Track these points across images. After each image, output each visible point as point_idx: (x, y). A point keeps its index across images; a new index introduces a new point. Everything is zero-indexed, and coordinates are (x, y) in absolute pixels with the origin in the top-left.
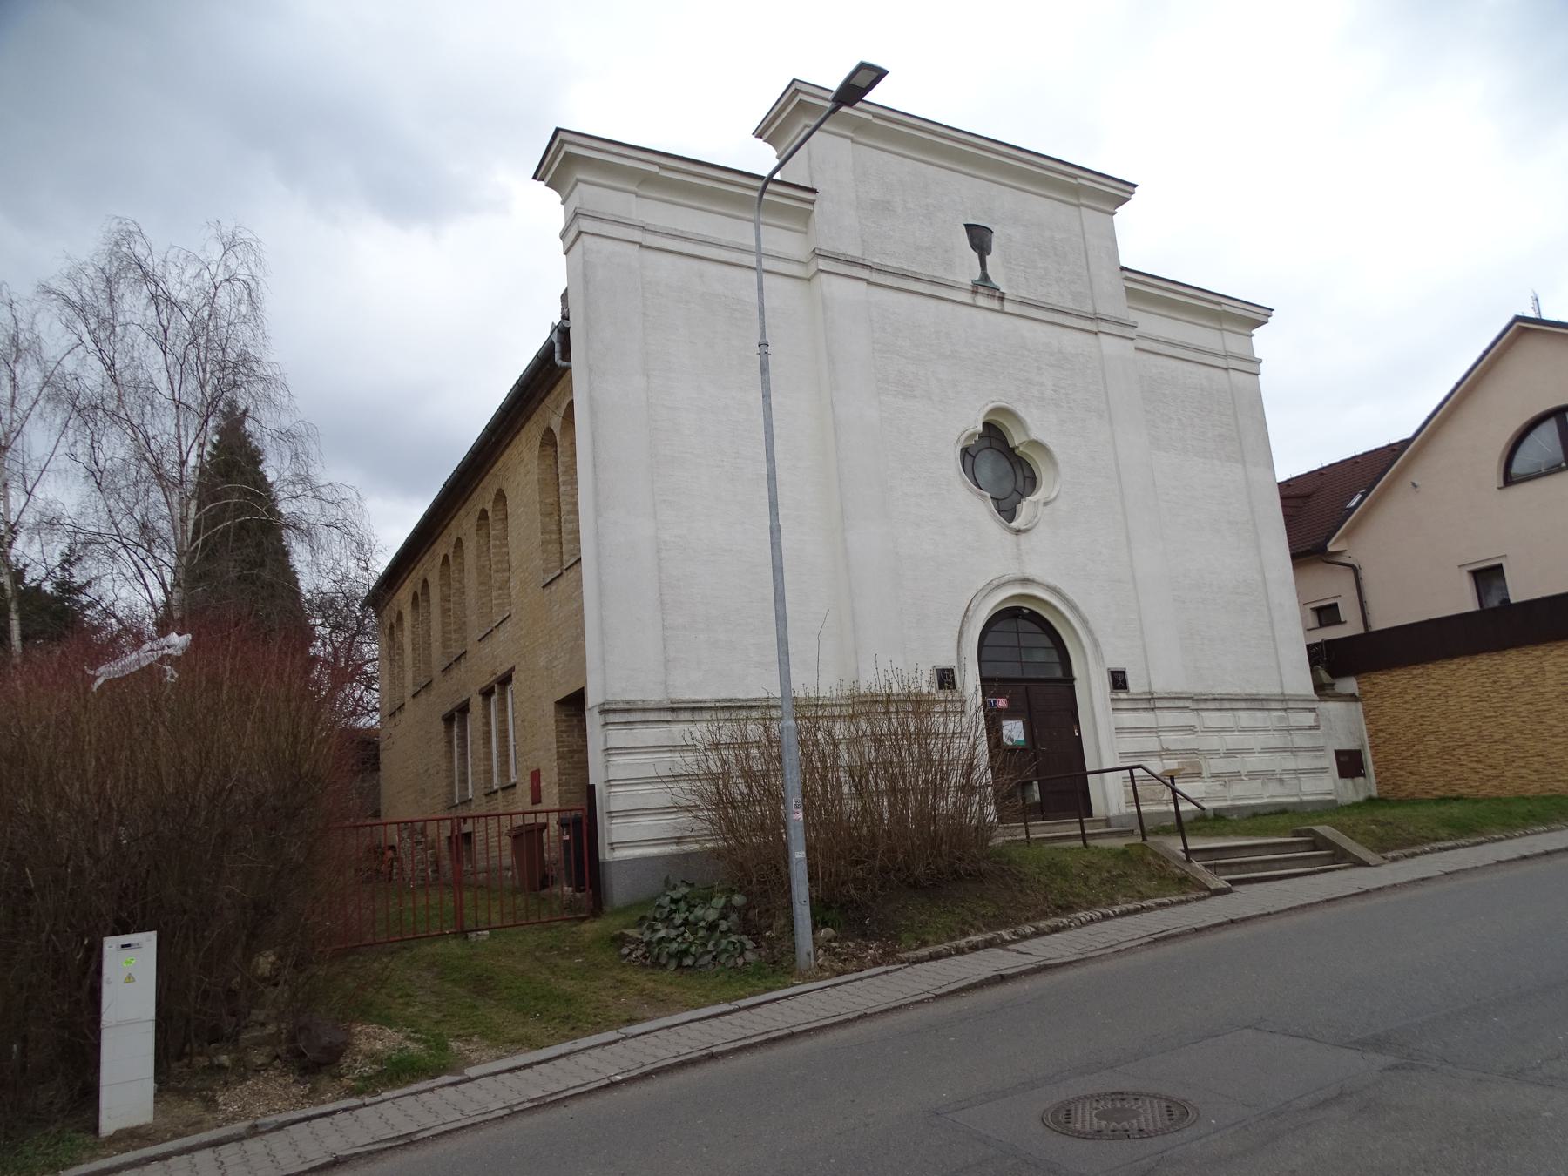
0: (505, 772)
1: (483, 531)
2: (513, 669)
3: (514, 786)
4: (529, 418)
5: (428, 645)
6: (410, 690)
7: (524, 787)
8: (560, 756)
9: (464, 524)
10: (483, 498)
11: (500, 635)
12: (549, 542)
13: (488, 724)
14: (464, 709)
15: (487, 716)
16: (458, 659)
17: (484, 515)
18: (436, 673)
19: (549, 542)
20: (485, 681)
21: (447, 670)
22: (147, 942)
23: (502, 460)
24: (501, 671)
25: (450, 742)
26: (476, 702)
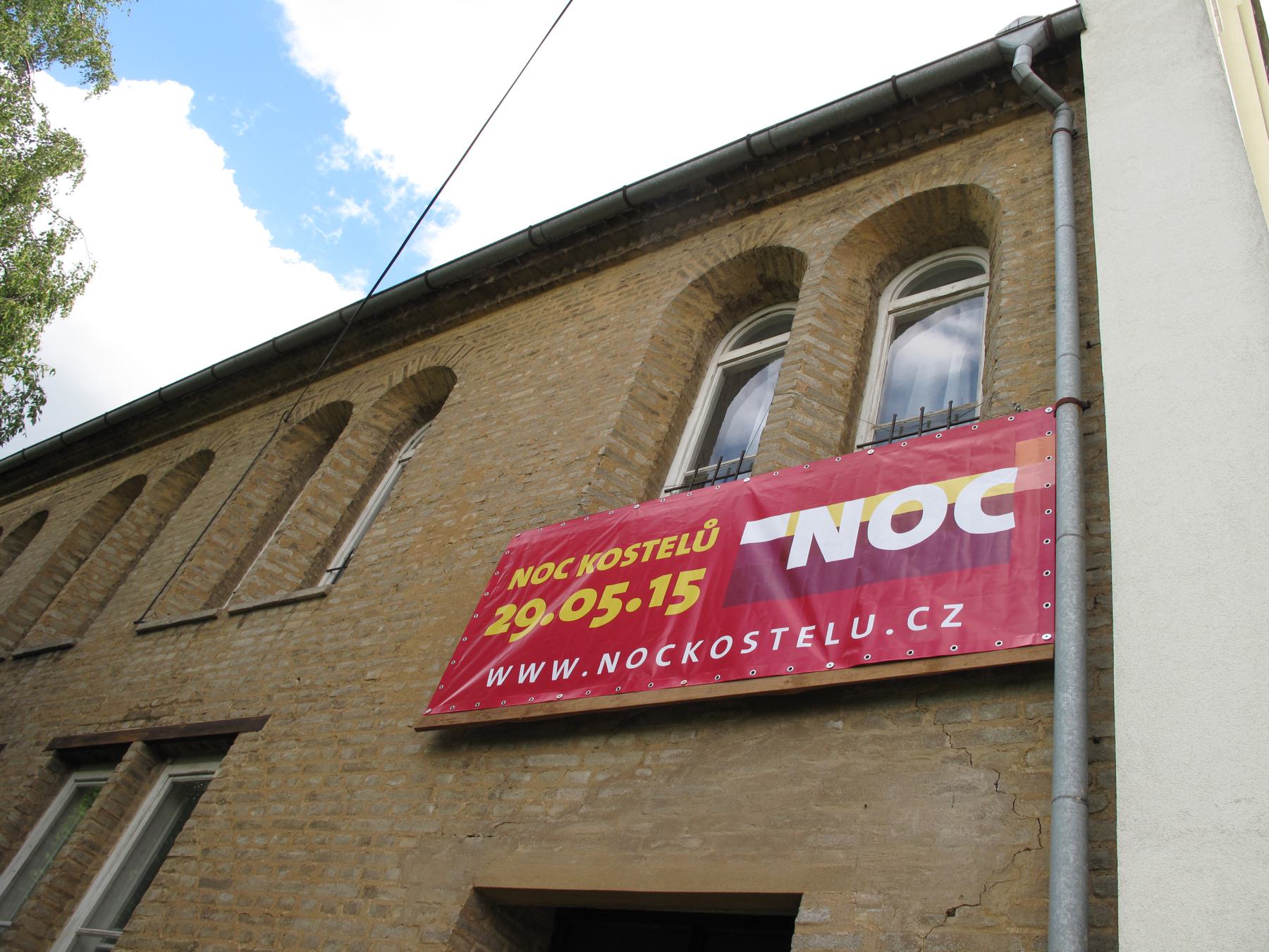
2: (257, 724)
12: (626, 463)
16: (33, 655)
20: (86, 723)
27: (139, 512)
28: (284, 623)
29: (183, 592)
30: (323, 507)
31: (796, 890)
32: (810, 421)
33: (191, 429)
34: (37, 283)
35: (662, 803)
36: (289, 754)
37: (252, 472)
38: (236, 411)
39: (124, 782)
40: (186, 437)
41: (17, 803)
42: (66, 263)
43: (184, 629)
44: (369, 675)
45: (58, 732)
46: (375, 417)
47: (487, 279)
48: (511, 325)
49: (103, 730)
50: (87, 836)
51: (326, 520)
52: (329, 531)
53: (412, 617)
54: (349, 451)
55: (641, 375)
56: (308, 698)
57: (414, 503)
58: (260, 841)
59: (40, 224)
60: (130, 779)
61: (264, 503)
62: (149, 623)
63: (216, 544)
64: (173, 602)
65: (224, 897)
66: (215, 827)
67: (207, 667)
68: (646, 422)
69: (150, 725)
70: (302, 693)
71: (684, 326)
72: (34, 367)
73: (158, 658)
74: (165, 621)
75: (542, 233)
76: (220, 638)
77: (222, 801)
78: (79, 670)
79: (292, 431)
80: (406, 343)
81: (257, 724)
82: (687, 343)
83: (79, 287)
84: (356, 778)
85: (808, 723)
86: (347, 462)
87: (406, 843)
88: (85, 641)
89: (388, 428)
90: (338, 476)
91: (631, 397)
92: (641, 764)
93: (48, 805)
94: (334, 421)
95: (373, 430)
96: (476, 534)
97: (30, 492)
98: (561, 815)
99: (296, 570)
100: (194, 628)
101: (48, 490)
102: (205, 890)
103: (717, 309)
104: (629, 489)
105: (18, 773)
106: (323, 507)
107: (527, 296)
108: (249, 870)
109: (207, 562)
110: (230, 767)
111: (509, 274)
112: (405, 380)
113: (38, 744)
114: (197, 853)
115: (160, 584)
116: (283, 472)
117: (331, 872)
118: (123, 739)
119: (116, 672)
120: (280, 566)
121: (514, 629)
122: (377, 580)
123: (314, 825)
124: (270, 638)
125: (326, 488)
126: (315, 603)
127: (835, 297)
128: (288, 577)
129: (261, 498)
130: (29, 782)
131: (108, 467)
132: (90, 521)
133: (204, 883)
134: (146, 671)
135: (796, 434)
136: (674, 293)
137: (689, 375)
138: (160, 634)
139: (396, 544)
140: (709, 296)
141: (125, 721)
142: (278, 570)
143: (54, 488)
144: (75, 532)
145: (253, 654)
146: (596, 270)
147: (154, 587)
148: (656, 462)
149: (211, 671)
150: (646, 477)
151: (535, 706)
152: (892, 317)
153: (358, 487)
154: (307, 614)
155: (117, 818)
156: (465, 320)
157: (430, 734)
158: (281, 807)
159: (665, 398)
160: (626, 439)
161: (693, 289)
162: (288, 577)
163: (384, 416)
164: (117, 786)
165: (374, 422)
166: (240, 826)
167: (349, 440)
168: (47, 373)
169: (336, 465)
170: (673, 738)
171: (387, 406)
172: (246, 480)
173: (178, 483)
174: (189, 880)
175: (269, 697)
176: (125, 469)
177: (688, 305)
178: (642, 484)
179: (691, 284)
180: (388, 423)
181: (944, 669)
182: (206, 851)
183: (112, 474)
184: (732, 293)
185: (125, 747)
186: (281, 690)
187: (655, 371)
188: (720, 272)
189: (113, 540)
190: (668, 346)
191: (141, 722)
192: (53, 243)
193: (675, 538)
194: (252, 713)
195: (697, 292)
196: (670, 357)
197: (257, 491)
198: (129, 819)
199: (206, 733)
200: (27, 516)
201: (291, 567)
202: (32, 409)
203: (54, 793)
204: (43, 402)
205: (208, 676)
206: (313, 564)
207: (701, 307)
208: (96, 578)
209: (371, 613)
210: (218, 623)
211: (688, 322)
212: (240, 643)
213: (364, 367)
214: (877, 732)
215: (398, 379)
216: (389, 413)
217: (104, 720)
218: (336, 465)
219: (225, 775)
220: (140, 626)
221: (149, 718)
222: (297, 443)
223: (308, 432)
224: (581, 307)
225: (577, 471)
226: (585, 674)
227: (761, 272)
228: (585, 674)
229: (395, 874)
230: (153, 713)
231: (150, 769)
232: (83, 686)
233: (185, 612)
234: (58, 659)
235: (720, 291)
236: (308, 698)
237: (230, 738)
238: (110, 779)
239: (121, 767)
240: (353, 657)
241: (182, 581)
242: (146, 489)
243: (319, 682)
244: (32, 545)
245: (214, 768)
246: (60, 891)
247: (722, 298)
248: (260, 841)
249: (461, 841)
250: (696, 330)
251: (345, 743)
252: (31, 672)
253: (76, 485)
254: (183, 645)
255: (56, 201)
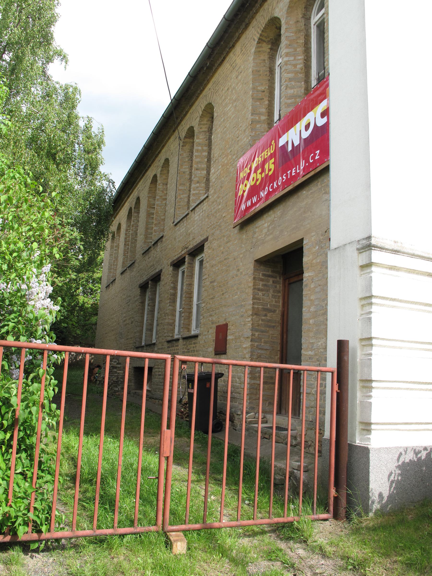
0: (188, 327)
1: (188, 147)
2: (206, 240)
3: (196, 337)
4: (247, 26)
5: (134, 241)
6: (120, 269)
7: (209, 337)
8: (256, 313)
9: (172, 148)
10: (193, 118)
11: (196, 216)
12: (259, 122)
13: (175, 288)
14: (156, 279)
15: (175, 282)
16: (156, 243)
17: (155, 179)
18: (138, 255)
19: (259, 122)
20: (175, 256)
21: (146, 252)
22: (207, 387)
23: (213, 80)
24: (192, 245)
25: (143, 303)
26: (168, 271)
27: (160, 187)
28: (203, 209)
29: (180, 208)
30: (200, 166)
31: (301, 238)
32: (292, 91)
33: (159, 152)
34: (92, 144)
35: (279, 226)
36: (215, 244)
37: (180, 162)
38: (167, 141)
39: (189, 266)
40: (160, 155)
41: (171, 282)
42: (95, 130)
43: (183, 220)
44: (223, 216)
45: (170, 261)
46: (201, 128)
47: (207, 64)
48: (220, 79)
49: (179, 256)
50: (187, 283)
51: (203, 169)
52: (205, 172)
53: (226, 195)
54: (199, 144)
55: (254, 88)
56: (214, 228)
57: (217, 158)
58: (217, 268)
59: (82, 124)
60: (189, 265)
61: (188, 170)
62: (176, 222)
63: (181, 190)
64: (179, 212)
65: (215, 284)
66: (208, 269)
67: (192, 229)
68: (260, 104)
69: (187, 250)
70: (212, 227)
71: (262, 60)
72: (106, 175)
73: (182, 231)
74: (179, 220)
75: (211, 44)
76: (192, 219)
77: (207, 262)
78: (167, 242)
79: (183, 142)
80: (198, 97)
81: (206, 240)
82: (264, 66)
83: (102, 136)
84: (228, 244)
85: (299, 194)
86: (200, 148)
87: (241, 256)
88: (165, 233)
89: (206, 129)
90: (199, 154)
91: (253, 99)
92: (275, 217)
93: (178, 279)
94: (191, 133)
95: (202, 133)
96: (232, 162)
97: (132, 192)
98: (265, 236)
99: (202, 189)
100: (185, 219)
101: (135, 190)
102: (211, 284)
103: (270, 46)
104: (263, 130)
105: (168, 275)
106: (200, 166)
107: (220, 65)
108: (217, 276)
109: (182, 196)
110: (206, 253)
111: (212, 59)
112: (202, 112)
113: (168, 265)
114: (207, 277)
115: (173, 209)
116: (188, 157)
117: (231, 269)
118: (183, 256)
119: (175, 239)
120: (197, 190)
121: (244, 191)
122: (217, 186)
123: (225, 260)
124: (201, 214)
125: (198, 160)
126: (207, 200)
127: (292, 34)
128: (201, 192)
129: (185, 168)
130: (171, 276)
131: (146, 175)
132: (150, 195)
133: (211, 282)
134: (181, 236)
135: (289, 99)
136: (253, 50)
137: (269, 78)
138: (179, 224)
139: (217, 173)
140: (265, 43)
141: (182, 251)
142: (197, 192)
143: (137, 188)
144: (148, 201)
145: (200, 220)
146: (233, 46)
147: (173, 210)
148: (268, 116)
149: (194, 229)
150: (266, 123)
151: (253, 210)
152: (315, 26)
153: (207, 154)
154: (206, 204)
155: (192, 276)
156: (208, 81)
157: (238, 227)
158: (218, 258)
159: (264, 91)
160: (256, 114)
161: (258, 45)
162: (201, 192)
163: (203, 126)
164: (188, 268)
165: (201, 130)
166: (212, 266)
167: (197, 141)
168: (110, 175)
169: (197, 151)
170: (279, 208)
171: (202, 123)
172: (179, 165)
173: (165, 172)
174: (208, 283)
175: (207, 231)
176: (150, 174)
177: (259, 51)
178: (266, 126)
179: (257, 44)
180: (205, 128)
181: (317, 172)
182: (209, 275)
183: (148, 177)
184: (271, 38)
185: (184, 258)
186: (208, 228)
187: (257, 84)
188: (263, 34)
189: (158, 199)
190: (259, 71)
191: (185, 250)
192: (87, 128)
193: (267, 150)
194: (205, 237)
195: (260, 45)
196: (260, 75)
197: (184, 167)
198: (194, 274)
199: (198, 247)
200: (135, 201)
201: (201, 189)
202: (113, 186)
203: (178, 276)
204: (114, 182)
205: (193, 231)
206: (206, 184)
207: (264, 49)
208: (160, 212)
209: (218, 197)
210: (190, 214)
211: (262, 57)
212: (196, 219)
213: (191, 111)
214: (311, 191)
215: (201, 113)
216: (204, 125)
217: (178, 253)
218: (197, 151)
219: (205, 256)
220: (174, 224)
221: (187, 248)
222: (187, 145)
223: (187, 140)
224: (234, 64)
225: (247, 133)
226: (307, 164)
227: (275, 26)
228: (307, 164)
229: (241, 264)
230: (187, 246)
231: (193, 261)
232: (170, 246)
233: (184, 213)
234: (162, 241)
235: (267, 39)
236: (214, 228)
237: (203, 246)
238: (185, 267)
239: (186, 263)
240: (219, 212)
241: (178, 205)
242: (158, 178)
243: (215, 222)
244: (141, 210)
245: (203, 255)
246: (188, 297)
247: (269, 41)
248: (217, 268)
249: (250, 251)
250: (266, 59)
251: (224, 236)
252: (158, 247)
253: (141, 185)
254: (185, 225)
255: (80, 115)
